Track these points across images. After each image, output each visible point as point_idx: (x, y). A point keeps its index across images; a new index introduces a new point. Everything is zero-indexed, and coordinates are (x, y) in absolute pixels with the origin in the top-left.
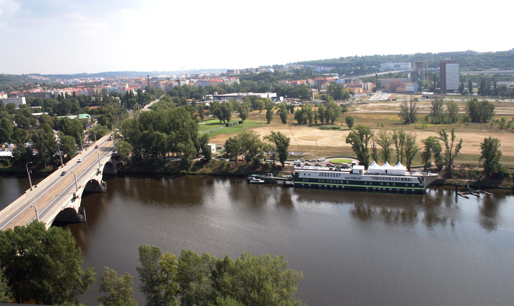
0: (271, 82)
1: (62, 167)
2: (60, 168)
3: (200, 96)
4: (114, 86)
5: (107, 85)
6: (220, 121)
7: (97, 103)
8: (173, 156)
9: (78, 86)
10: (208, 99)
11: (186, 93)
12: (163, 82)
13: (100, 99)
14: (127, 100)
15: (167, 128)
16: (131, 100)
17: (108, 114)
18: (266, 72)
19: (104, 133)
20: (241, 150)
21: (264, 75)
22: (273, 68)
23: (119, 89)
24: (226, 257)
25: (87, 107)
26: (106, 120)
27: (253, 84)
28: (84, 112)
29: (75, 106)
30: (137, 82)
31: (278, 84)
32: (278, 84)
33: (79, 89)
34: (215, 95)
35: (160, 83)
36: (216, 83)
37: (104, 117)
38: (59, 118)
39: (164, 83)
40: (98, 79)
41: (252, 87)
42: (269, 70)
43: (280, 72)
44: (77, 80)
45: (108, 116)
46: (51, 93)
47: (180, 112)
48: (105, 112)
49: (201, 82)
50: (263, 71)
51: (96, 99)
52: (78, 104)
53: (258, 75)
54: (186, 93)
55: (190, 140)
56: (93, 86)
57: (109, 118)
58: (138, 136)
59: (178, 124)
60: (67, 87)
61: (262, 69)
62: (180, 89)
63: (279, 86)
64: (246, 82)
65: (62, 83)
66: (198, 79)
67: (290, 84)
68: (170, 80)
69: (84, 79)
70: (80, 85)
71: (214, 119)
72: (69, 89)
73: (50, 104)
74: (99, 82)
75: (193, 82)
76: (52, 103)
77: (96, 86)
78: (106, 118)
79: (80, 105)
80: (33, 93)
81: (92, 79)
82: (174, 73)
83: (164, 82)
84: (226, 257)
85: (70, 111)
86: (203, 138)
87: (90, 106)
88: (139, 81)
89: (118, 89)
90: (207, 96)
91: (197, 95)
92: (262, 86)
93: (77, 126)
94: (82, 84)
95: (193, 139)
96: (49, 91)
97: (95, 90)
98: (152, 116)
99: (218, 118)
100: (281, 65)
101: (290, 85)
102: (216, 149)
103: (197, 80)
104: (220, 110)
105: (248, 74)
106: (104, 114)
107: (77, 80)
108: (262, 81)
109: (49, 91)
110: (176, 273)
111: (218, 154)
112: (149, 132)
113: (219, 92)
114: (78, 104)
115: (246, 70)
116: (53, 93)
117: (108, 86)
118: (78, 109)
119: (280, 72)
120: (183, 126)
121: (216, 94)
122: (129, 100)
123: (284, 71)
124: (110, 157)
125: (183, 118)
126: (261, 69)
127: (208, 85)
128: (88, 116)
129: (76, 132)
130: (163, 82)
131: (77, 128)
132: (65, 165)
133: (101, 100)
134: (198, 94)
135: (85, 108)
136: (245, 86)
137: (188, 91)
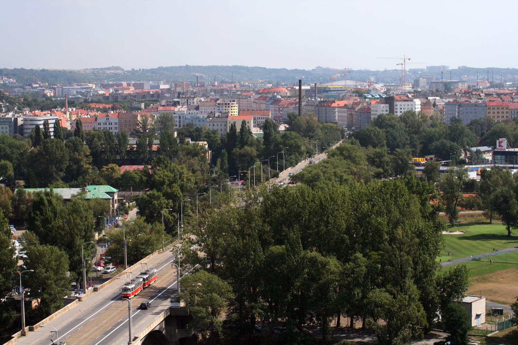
1: (23, 334)
2: (15, 335)
3: (452, 148)
4: (197, 108)
5: (176, 104)
6: (508, 229)
7: (142, 156)
8: (351, 329)
9: (93, 105)
10: (476, 158)
11: (411, 138)
12: (342, 103)
13: (150, 145)
14: (229, 152)
15: (343, 241)
16: (242, 151)
17: (169, 191)
19: (152, 245)
23: (209, 117)
25: (111, 165)
26: (162, 208)
28: (102, 180)
29: (77, 162)
30: (265, 98)
33: (93, 114)
34: (498, 149)
35: (333, 105)
36: (505, 111)
37: (158, 198)
38: (29, 194)
39: (346, 106)
40: (152, 87)
44: (90, 85)
45: (168, 196)
46: (16, 120)
47: (388, 196)
48: (163, 183)
49: (460, 105)
51: (139, 145)
52: (87, 156)
54: (411, 138)
55: (409, 282)
56: (135, 104)
57: (170, 201)
58: (254, 262)
59: (378, 232)
60: (62, 105)
62: (393, 126)
65: (49, 93)
66: (450, 97)
68: (366, 98)
69: (112, 86)
70: (99, 102)
71: (490, 223)
72: (65, 113)
73: (8, 151)
74: (152, 96)
75: (434, 105)
76: (15, 150)
77: (143, 106)
78: (163, 200)
79: (91, 159)
81: (134, 85)
82: (380, 76)
83: (345, 102)
85: (62, 174)
86: (450, 279)
87: (121, 163)
88: (270, 96)
89: (206, 116)
90: (474, 149)
91: (443, 145)
93: (78, 221)
94: (106, 99)
95: (418, 281)
96: (10, 115)
97: (139, 118)
98: (301, 203)
99: (503, 220)
102: (488, 315)
103: (447, 100)
104: (511, 197)
106: (159, 190)
107: (90, 85)
109: (10, 115)
111: (492, 332)
112: (287, 249)
113: (512, 139)
114: (87, 156)
116: (20, 122)
117: (177, 109)
118: (86, 172)
120: (393, 240)
121: (503, 145)
122: (237, 150)
124: (161, 318)
125: (396, 214)
127: (480, 115)
128: (111, 194)
129: (72, 235)
130: (342, 103)
131: (76, 225)
132: (31, 330)
133: (155, 148)
134: (448, 143)
135: (105, 168)
137: (416, 133)
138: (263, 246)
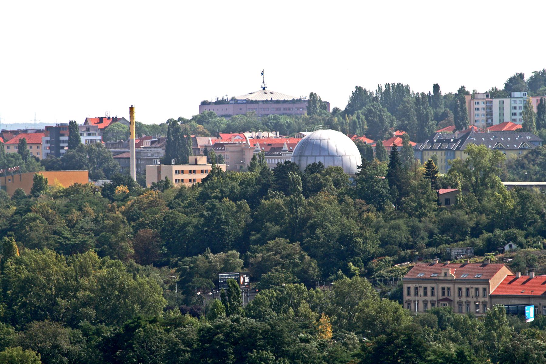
0: (324, 279)
18: (272, 163)
20: (138, 298)
21: (254, 201)
22: (350, 132)
24: (132, 106)
27: (124, 292)
31: (398, 296)
32: (398, 296)
41: (108, 331)
42: (308, 143)
43: (430, 169)
50: (242, 150)
53: (181, 194)
61: (236, 138)
63: (406, 321)
64: (44, 268)
67: (529, 299)
80: (364, 125)
84: (132, 106)
92: (224, 319)
100: (460, 88)
101: (530, 313)
105: (76, 189)
108: (227, 267)
110: (379, 299)
115: (55, 145)
119: (430, 169)
123: (476, 156)
126: (225, 139)
136: (37, 317)
138: (77, 193)
